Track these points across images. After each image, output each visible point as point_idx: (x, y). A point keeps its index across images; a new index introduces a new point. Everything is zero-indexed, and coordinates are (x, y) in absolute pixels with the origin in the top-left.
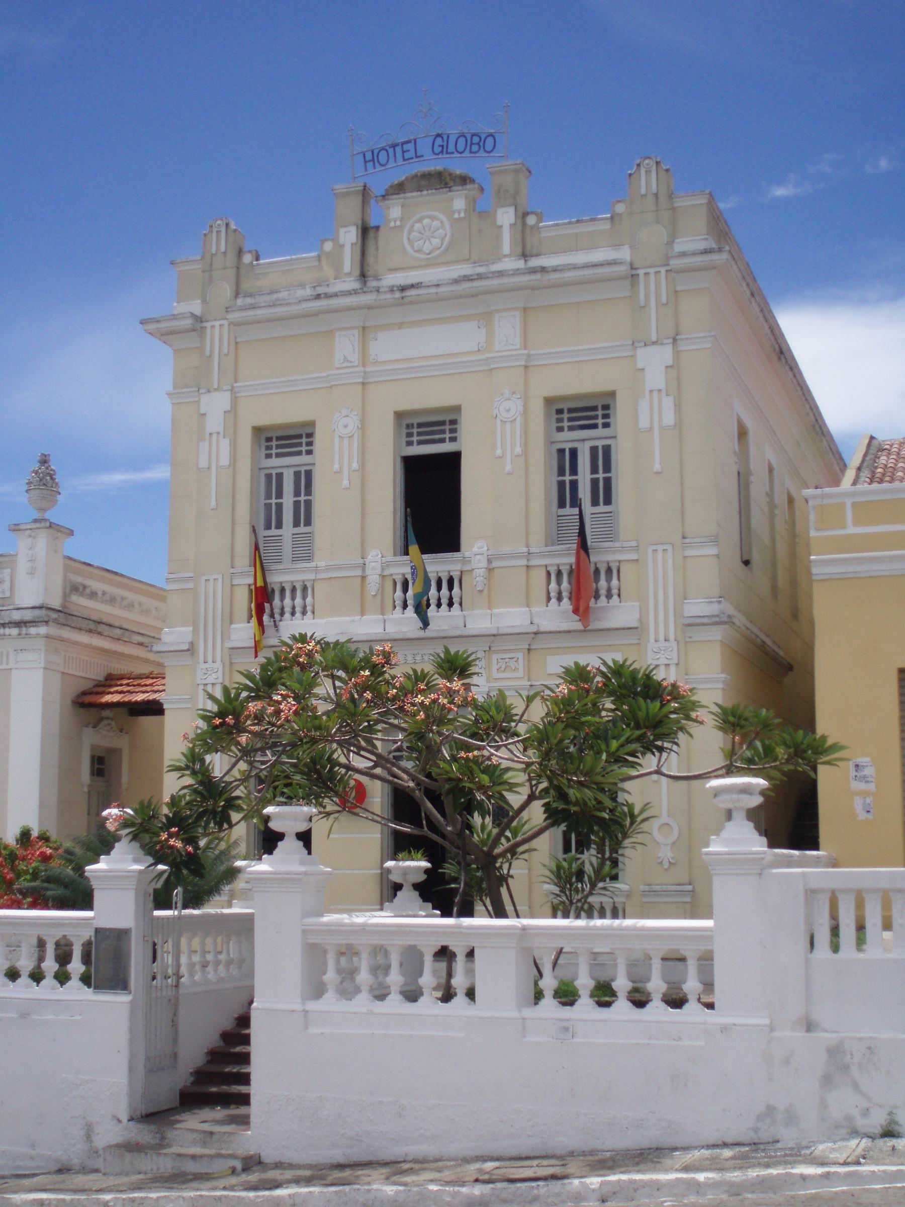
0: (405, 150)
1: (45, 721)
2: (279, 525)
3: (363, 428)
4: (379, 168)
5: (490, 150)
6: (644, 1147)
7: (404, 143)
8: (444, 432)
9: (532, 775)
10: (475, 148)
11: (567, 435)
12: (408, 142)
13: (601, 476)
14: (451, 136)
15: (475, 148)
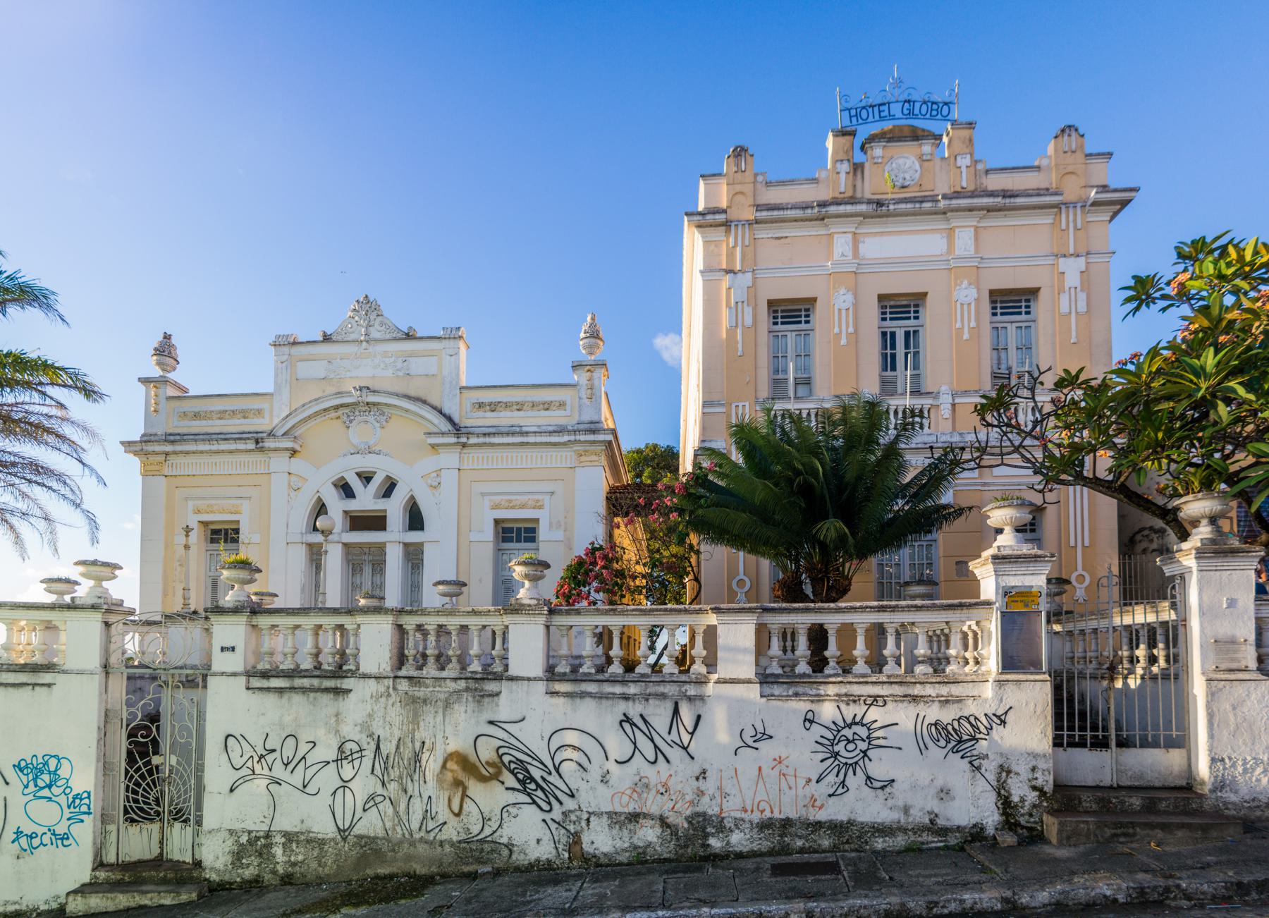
2: (894, 368)
3: (855, 305)
8: (800, 316)
10: (934, 113)
11: (888, 323)
12: (884, 104)
13: (889, 351)
15: (934, 113)
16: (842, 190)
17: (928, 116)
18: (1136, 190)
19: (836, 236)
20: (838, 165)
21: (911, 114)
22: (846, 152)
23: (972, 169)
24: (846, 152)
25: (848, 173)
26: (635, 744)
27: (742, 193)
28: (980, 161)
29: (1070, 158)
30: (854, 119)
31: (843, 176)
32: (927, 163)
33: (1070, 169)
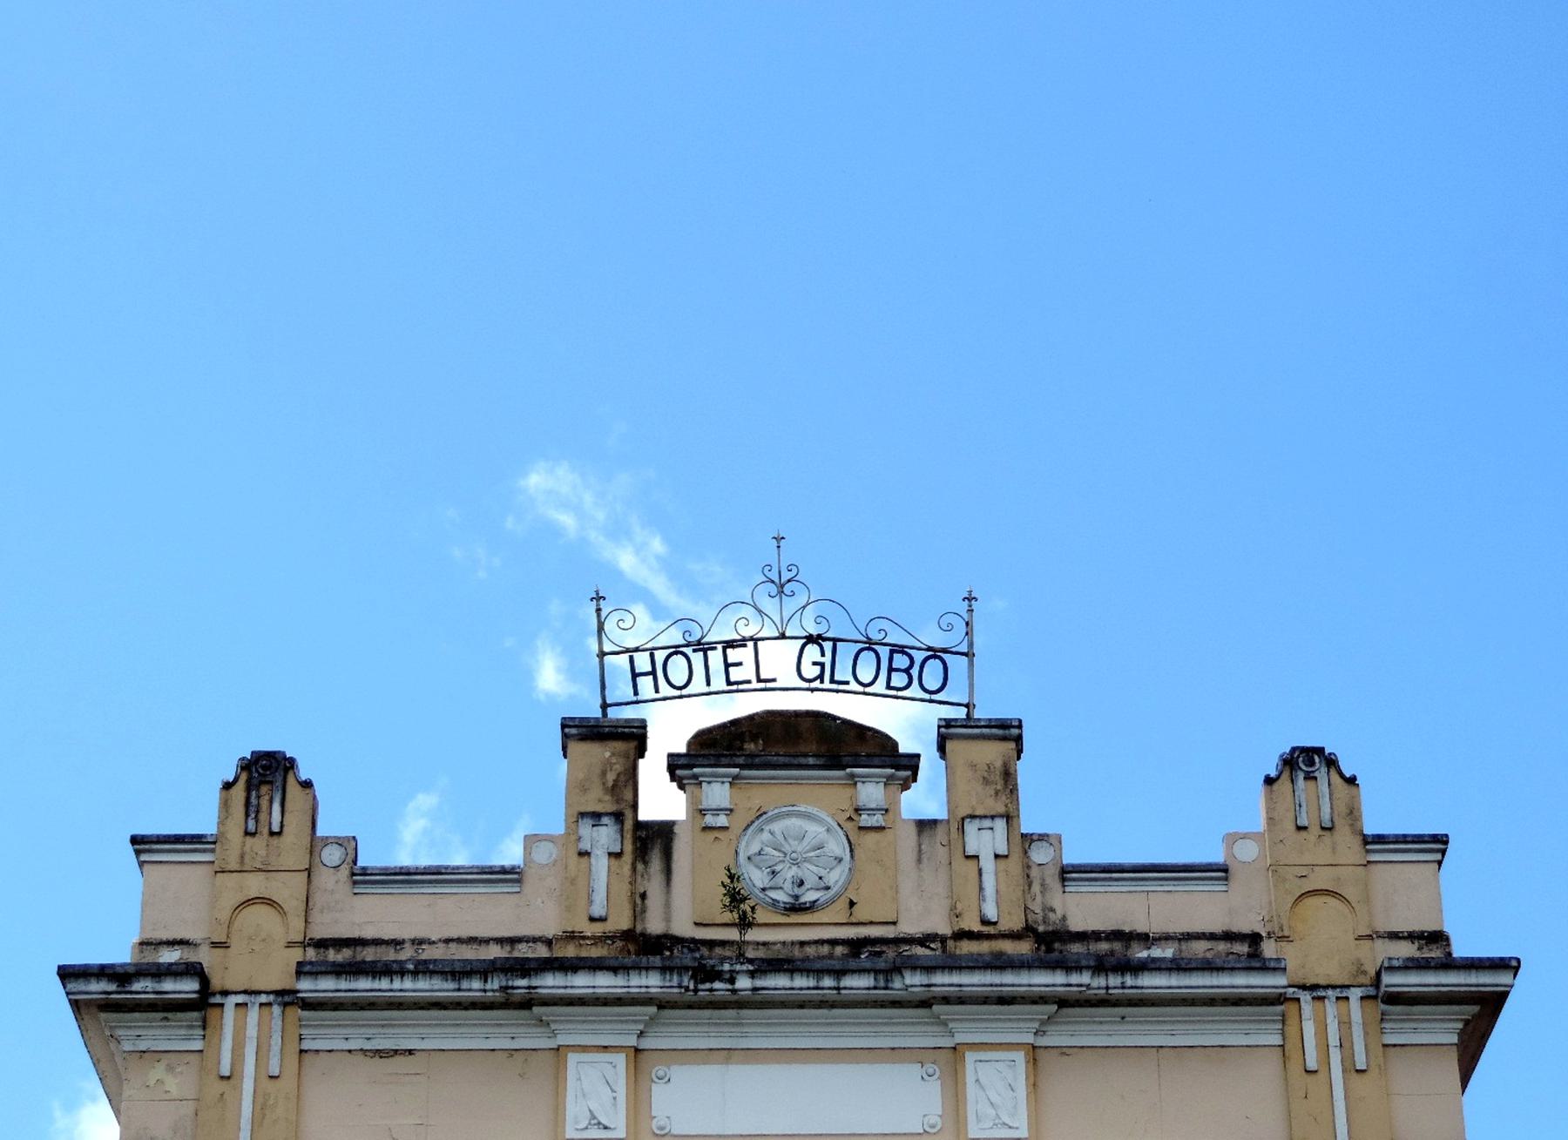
0: (730, 660)
1: (695, 1068)
4: (915, 691)
5: (681, 684)
6: (277, 913)
7: (730, 644)
9: (668, 953)
10: (899, 680)
14: (657, 653)
15: (899, 680)
16: (598, 911)
17: (880, 686)
18: (1509, 965)
19: (573, 1058)
20: (585, 829)
21: (826, 678)
22: (614, 790)
23: (1014, 865)
24: (614, 790)
25: (616, 856)
26: (804, 607)
27: (270, 902)
28: (1043, 837)
29: (1316, 850)
30: (646, 684)
31: (601, 864)
32: (871, 837)
33: (1320, 880)
